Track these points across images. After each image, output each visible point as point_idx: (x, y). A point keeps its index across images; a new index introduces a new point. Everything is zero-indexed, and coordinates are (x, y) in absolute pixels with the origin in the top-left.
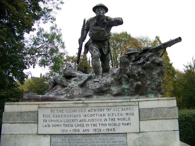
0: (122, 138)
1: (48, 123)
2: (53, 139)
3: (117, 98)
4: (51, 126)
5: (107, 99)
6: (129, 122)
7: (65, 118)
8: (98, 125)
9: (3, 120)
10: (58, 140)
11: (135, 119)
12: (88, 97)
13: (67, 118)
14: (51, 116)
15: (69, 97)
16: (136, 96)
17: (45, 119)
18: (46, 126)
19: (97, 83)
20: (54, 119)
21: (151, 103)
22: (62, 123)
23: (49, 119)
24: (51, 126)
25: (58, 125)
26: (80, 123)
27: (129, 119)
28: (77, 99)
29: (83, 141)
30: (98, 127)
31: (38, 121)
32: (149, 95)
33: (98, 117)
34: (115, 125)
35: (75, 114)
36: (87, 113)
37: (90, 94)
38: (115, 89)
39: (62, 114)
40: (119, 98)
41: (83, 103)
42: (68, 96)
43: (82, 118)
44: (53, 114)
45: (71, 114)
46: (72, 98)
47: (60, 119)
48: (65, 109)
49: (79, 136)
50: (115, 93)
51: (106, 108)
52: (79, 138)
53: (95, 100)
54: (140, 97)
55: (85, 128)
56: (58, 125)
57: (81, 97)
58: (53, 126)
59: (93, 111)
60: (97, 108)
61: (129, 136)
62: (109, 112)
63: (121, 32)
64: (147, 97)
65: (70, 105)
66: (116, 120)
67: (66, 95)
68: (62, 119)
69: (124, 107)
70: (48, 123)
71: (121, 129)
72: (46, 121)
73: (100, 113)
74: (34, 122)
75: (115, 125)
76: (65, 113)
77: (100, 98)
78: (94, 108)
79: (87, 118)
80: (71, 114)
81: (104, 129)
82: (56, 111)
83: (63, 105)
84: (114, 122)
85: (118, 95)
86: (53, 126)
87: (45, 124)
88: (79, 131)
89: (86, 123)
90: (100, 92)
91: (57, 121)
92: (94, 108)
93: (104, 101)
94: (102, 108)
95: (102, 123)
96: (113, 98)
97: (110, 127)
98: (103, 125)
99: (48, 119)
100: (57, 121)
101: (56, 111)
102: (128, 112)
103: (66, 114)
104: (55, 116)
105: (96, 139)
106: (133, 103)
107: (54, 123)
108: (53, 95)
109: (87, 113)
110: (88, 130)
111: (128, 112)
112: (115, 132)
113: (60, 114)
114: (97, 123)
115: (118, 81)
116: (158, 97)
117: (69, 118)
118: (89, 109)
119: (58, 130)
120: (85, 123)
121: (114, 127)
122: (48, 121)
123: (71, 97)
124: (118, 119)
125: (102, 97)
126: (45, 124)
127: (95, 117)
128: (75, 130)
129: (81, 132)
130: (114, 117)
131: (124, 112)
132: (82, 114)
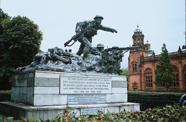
0: (104, 97)
1: (66, 87)
2: (69, 97)
3: (98, 73)
4: (68, 89)
5: (92, 73)
6: (107, 88)
7: (76, 84)
8: (93, 89)
9: (35, 84)
10: (72, 98)
11: (110, 86)
12: (84, 71)
13: (78, 84)
14: (68, 82)
15: (73, 71)
16: (107, 74)
17: (64, 84)
18: (65, 89)
19: (88, 63)
20: (71, 84)
21: (115, 78)
22: (75, 87)
23: (67, 84)
24: (68, 89)
25: (72, 88)
26: (84, 87)
27: (107, 86)
28: (78, 72)
29: (85, 98)
30: (94, 90)
31: (60, 85)
32: (113, 73)
33: (93, 84)
34: (101, 89)
35: (82, 81)
36: (88, 81)
37: (85, 69)
38: (98, 68)
39: (75, 81)
40: (100, 73)
41: (142, 82)
42: (74, 69)
43: (86, 84)
44: (70, 81)
45: (80, 81)
46: (75, 71)
47: (73, 84)
48: (76, 78)
49: (83, 95)
50: (98, 70)
51: (97, 79)
52: (83, 96)
53: (87, 73)
54: (109, 74)
55: (87, 90)
56: (72, 88)
57: (80, 71)
58: (70, 89)
59: (91, 80)
60: (93, 79)
61: (107, 95)
62: (99, 82)
63: (16, 16)
64: (112, 74)
65: (77, 75)
66: (102, 86)
67: (72, 69)
68: (75, 84)
69: (106, 79)
70: (66, 87)
71: (103, 92)
72: (65, 85)
73: (95, 81)
74: (57, 86)
75: (101, 89)
76: (76, 81)
77: (90, 73)
78: (92, 79)
79: (88, 84)
80: (80, 81)
81: (96, 91)
82: (71, 79)
83: (73, 75)
84: (101, 87)
85: (99, 72)
86: (70, 89)
87: (65, 87)
88: (84, 92)
89: (88, 87)
90: (90, 69)
91: (72, 85)
92: (92, 79)
93: (92, 75)
94: (96, 79)
95: (95, 87)
96: (97, 73)
97: (99, 90)
98: (95, 89)
99: (66, 84)
100: (72, 85)
101: (71, 79)
102: (107, 82)
103: (77, 81)
104: (71, 82)
105: (92, 97)
106: (109, 77)
107: (70, 87)
108: (63, 68)
109: (88, 81)
110: (88, 92)
111: (107, 82)
112: (101, 93)
113: (74, 81)
114: (93, 87)
115: (100, 64)
116: (116, 75)
117: (79, 84)
118: (89, 79)
119: (72, 92)
120: (87, 87)
121: (101, 90)
122: (66, 85)
123: (74, 71)
124: (103, 86)
125: (90, 72)
126: (65, 87)
127: (92, 84)
128: (82, 92)
129: (85, 93)
130: (101, 84)
131: (105, 82)
132: (86, 82)
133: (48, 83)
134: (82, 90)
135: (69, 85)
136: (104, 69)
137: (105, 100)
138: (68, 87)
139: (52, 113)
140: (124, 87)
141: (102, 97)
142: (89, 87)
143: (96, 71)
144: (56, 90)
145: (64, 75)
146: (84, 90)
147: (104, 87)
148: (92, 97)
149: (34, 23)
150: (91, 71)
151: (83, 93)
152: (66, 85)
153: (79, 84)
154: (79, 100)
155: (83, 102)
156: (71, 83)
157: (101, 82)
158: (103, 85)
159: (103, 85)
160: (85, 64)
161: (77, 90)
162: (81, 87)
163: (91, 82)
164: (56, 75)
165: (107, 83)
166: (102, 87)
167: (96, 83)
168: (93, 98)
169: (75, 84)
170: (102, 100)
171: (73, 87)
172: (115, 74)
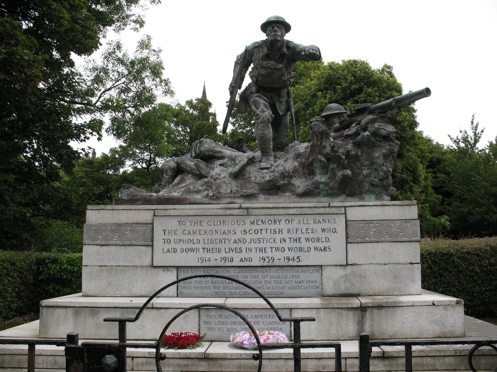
0: (314, 276)
3: (303, 199)
4: (179, 251)
6: (327, 245)
8: (268, 250)
9: (84, 239)
13: (210, 237)
15: (211, 198)
17: (167, 237)
18: (168, 251)
23: (175, 237)
24: (179, 251)
25: (192, 250)
26: (233, 246)
31: (153, 241)
33: (269, 236)
34: (301, 249)
35: (225, 228)
38: (300, 184)
39: (201, 228)
40: (308, 199)
43: (239, 236)
44: (183, 228)
46: (218, 198)
47: (195, 237)
50: (300, 190)
51: (283, 218)
55: (244, 255)
56: (192, 250)
58: (182, 251)
59: (260, 222)
61: (327, 272)
62: (290, 226)
64: (363, 199)
65: (186, 211)
66: (303, 240)
67: (205, 193)
74: (145, 243)
75: (301, 249)
77: (271, 200)
79: (248, 237)
81: (279, 258)
82: (188, 223)
83: (196, 211)
84: (298, 245)
85: (306, 194)
86: (182, 251)
87: (167, 246)
89: (247, 245)
90: (273, 188)
96: (298, 199)
97: (291, 255)
98: (277, 249)
101: (188, 223)
105: (264, 277)
106: (335, 210)
107: (184, 246)
108: (180, 194)
110: (250, 260)
111: (326, 226)
114: (268, 245)
117: (214, 237)
121: (298, 254)
123: (216, 198)
124: (307, 240)
126: (167, 246)
128: (225, 259)
129: (236, 263)
131: (318, 227)
133: (119, 235)
134: (226, 255)
135: (180, 241)
136: (321, 183)
137: (318, 284)
138: (179, 246)
139: (95, 319)
140: (404, 239)
141: (305, 276)
142: (253, 245)
143: (293, 192)
144: (141, 256)
145: (168, 213)
146: (231, 255)
147: (311, 245)
148: (264, 277)
149: (415, 114)
150: (277, 194)
151: (230, 264)
152: (172, 241)
153: (214, 237)
154: (218, 285)
155: (233, 291)
156: (189, 233)
157: (299, 226)
158: (307, 236)
159: (310, 236)
160: (256, 173)
161: (207, 255)
162: (222, 246)
163: (258, 227)
164: (140, 214)
165: (323, 230)
166: (304, 244)
167: (289, 231)
168: (268, 279)
169: (200, 237)
170: (304, 284)
171: (194, 246)
172: (377, 199)
